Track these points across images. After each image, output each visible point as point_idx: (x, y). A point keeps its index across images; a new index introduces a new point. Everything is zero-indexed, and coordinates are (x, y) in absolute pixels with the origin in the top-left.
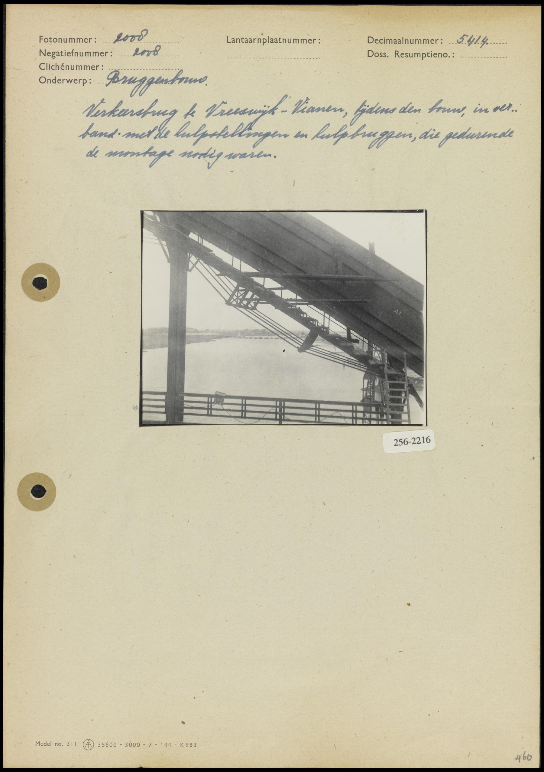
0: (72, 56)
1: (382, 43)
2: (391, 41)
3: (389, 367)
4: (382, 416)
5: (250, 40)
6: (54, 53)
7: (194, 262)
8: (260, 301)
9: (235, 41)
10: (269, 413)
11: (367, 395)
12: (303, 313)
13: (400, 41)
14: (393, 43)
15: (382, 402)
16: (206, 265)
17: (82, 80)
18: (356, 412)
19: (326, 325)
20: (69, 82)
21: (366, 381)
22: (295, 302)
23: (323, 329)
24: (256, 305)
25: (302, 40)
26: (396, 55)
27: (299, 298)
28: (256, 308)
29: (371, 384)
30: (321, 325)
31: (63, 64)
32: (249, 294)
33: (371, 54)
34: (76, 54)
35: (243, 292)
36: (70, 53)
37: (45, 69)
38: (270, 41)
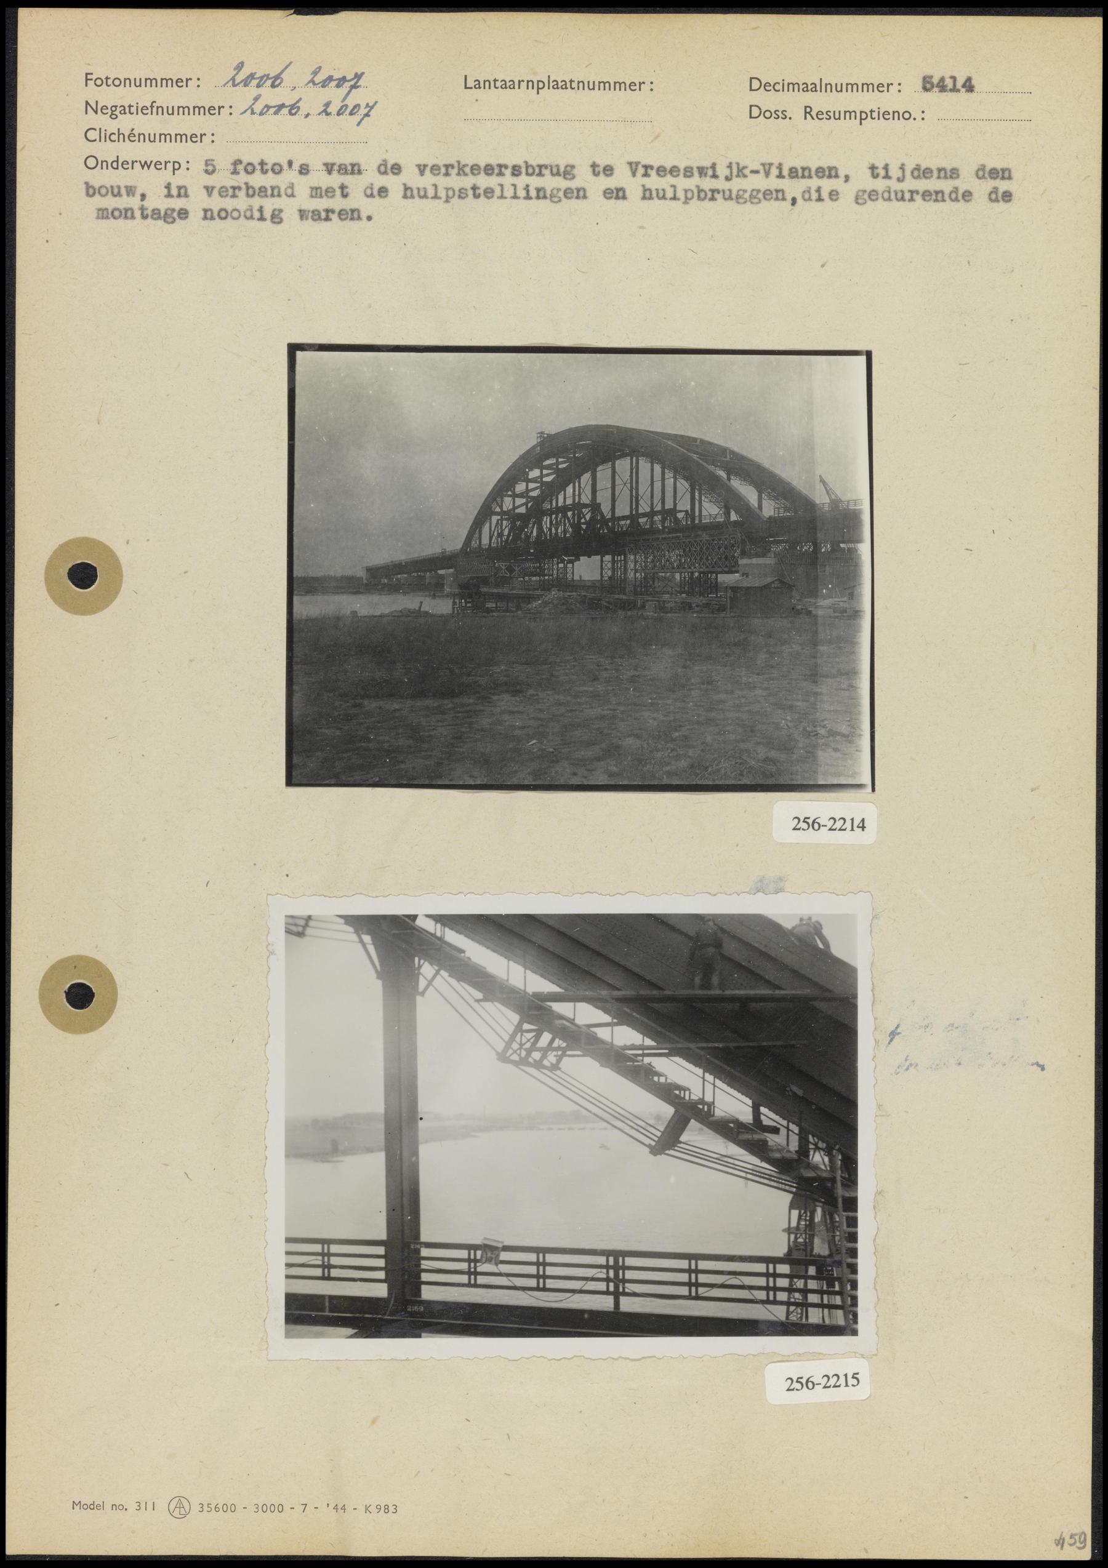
0: (152, 114)
1: (779, 91)
2: (796, 86)
3: (846, 1182)
4: (831, 1284)
5: (511, 83)
6: (114, 109)
7: (429, 976)
8: (569, 1053)
9: (482, 85)
10: (593, 1279)
11: (797, 1242)
12: (659, 1075)
13: (815, 87)
14: (801, 90)
15: (830, 1256)
16: (453, 981)
17: (172, 163)
18: (775, 1275)
19: (708, 1098)
20: (146, 167)
21: (795, 1213)
22: (640, 1052)
23: (701, 1107)
24: (559, 1061)
25: (619, 85)
26: (808, 115)
27: (649, 1042)
28: (560, 1066)
29: (806, 1220)
30: (697, 1098)
31: (133, 130)
32: (546, 1037)
33: (756, 113)
34: (160, 109)
35: (534, 1034)
36: (148, 109)
37: (95, 140)
38: (551, 84)
